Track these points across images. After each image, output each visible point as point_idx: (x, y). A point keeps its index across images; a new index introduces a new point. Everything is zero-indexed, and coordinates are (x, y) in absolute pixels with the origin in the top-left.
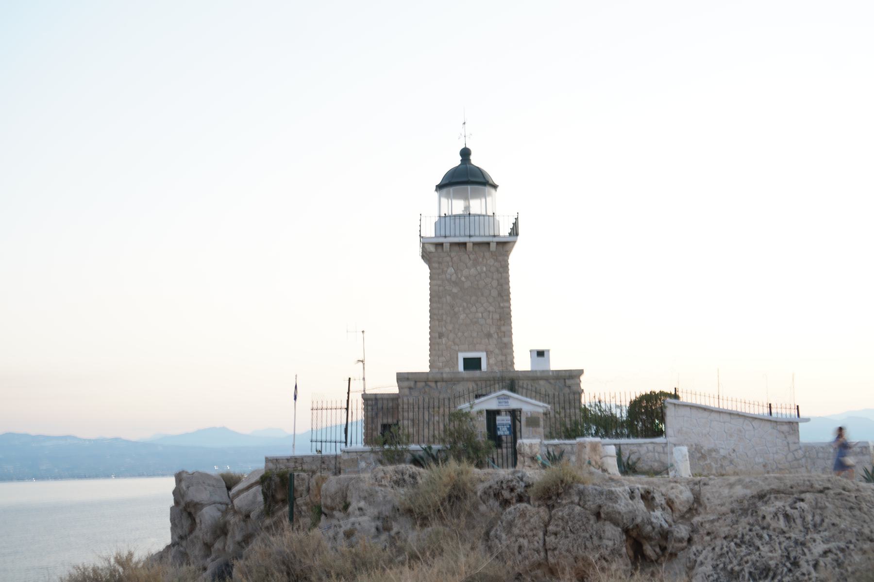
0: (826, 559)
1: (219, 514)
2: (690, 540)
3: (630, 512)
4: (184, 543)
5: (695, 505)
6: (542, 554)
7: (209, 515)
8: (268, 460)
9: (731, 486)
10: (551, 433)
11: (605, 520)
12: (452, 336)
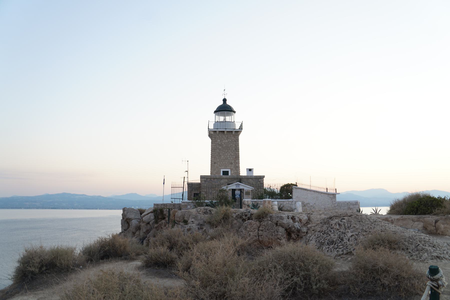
0: (352, 238)
1: (138, 222)
2: (307, 233)
3: (288, 223)
4: (126, 232)
5: (309, 221)
6: (257, 237)
7: (134, 223)
8: (154, 205)
9: (320, 215)
10: (253, 197)
11: (279, 226)
12: (219, 163)
